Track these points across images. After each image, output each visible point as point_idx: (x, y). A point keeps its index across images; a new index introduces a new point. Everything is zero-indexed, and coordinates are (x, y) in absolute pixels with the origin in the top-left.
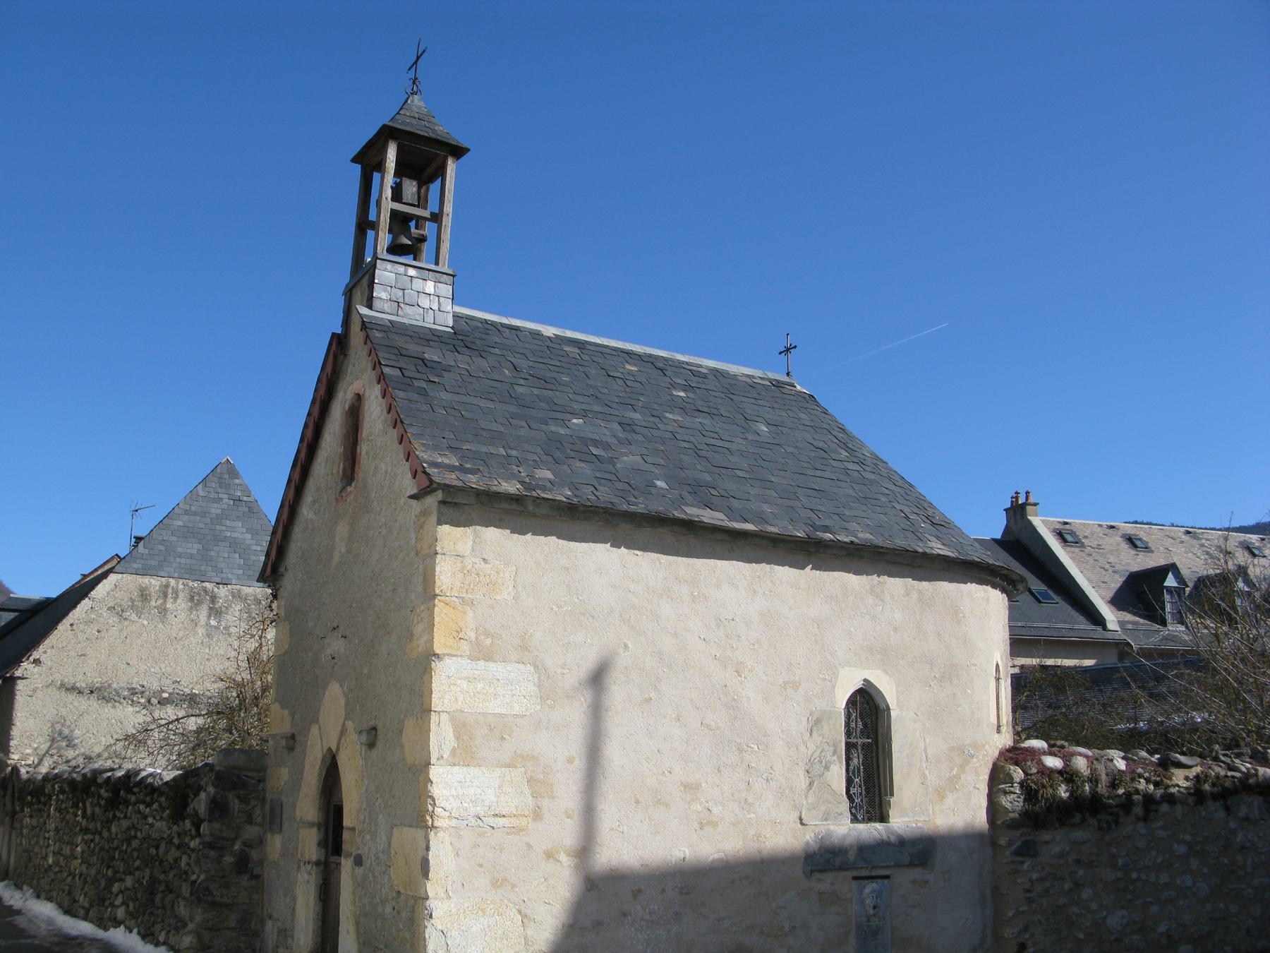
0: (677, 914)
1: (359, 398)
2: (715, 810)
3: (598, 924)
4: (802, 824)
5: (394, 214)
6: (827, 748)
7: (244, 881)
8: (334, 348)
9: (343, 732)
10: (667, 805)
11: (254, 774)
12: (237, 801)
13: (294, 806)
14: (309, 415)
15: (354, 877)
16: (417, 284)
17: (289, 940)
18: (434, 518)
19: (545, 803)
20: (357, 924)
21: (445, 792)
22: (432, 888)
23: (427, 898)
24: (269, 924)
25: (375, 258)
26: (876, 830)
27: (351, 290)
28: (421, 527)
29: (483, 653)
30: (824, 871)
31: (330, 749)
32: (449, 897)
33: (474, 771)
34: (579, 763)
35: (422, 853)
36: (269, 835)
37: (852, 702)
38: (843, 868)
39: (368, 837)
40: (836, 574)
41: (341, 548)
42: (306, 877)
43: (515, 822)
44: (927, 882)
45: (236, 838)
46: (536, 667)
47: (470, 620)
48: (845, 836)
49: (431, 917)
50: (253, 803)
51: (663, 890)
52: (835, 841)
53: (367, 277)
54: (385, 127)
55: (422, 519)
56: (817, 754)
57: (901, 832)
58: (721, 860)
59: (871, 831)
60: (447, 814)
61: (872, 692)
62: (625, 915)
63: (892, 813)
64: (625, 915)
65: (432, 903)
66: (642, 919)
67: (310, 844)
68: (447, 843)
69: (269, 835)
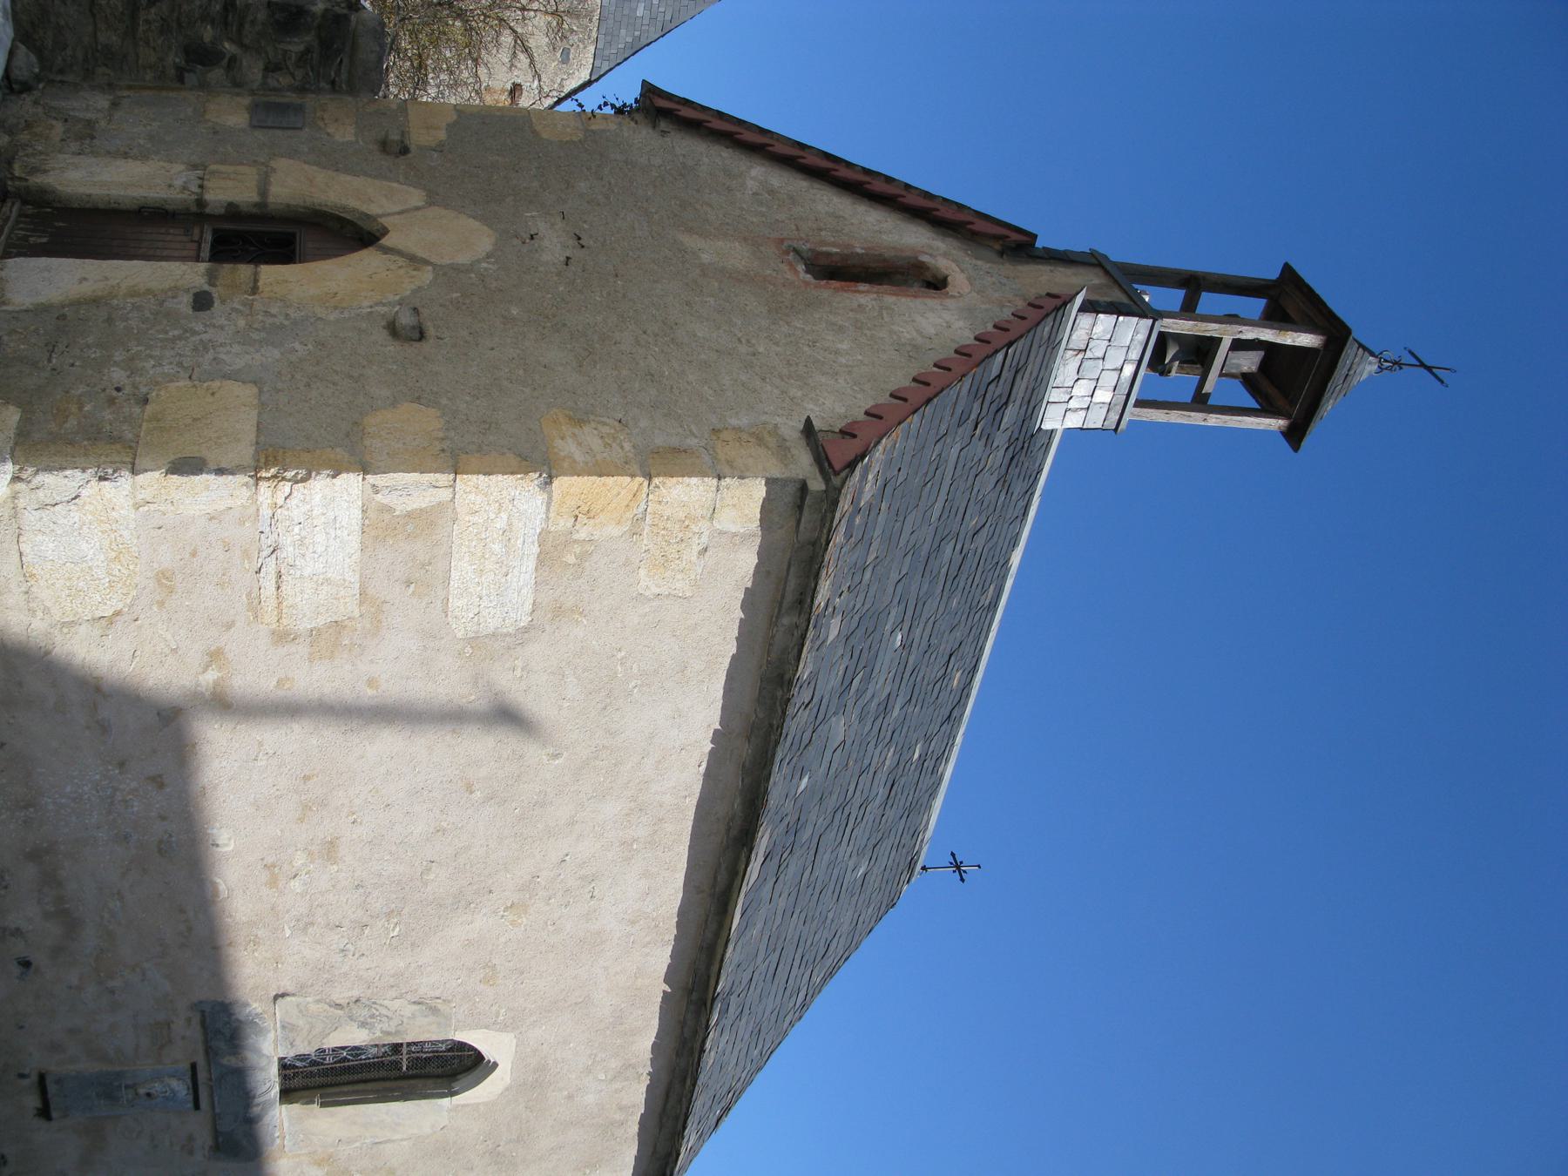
0: (126, 837)
1: (937, 284)
2: (296, 885)
3: (104, 728)
4: (276, 997)
5: (1215, 342)
6: (394, 1023)
7: (174, 58)
8: (1015, 236)
9: (414, 261)
10: (301, 820)
11: (344, 76)
12: (301, 48)
13: (292, 154)
14: (907, 186)
15: (175, 291)
16: (1109, 379)
17: (74, 146)
18: (776, 472)
19: (302, 649)
20: (95, 301)
21: (318, 498)
22: (152, 481)
23: (134, 472)
24: (103, 101)
25: (1156, 315)
26: (268, 1091)
27: (1100, 265)
28: (760, 441)
29: (550, 553)
30: (203, 1023)
31: (385, 232)
32: (137, 507)
33: (354, 542)
34: (368, 694)
35: (212, 457)
36: (246, 101)
37: (462, 1046)
38: (210, 1052)
39: (242, 323)
40: (655, 1023)
41: (709, 251)
42: (178, 183)
43: (270, 604)
44: (191, 1153)
45: (242, 45)
46: (526, 630)
47: (609, 530)
48: (258, 1051)
49: (102, 479)
50: (299, 74)
51: (163, 818)
52: (252, 1040)
53: (1125, 300)
54: (1347, 331)
55: (772, 442)
56: (384, 1012)
57: (267, 1119)
58: (216, 893)
59: (268, 1081)
60: (280, 501)
61: (477, 1072)
62: (121, 765)
63: (296, 1108)
64: (121, 765)
65: (125, 481)
66: (115, 789)
67: (232, 188)
68: (230, 502)
69: (246, 101)
